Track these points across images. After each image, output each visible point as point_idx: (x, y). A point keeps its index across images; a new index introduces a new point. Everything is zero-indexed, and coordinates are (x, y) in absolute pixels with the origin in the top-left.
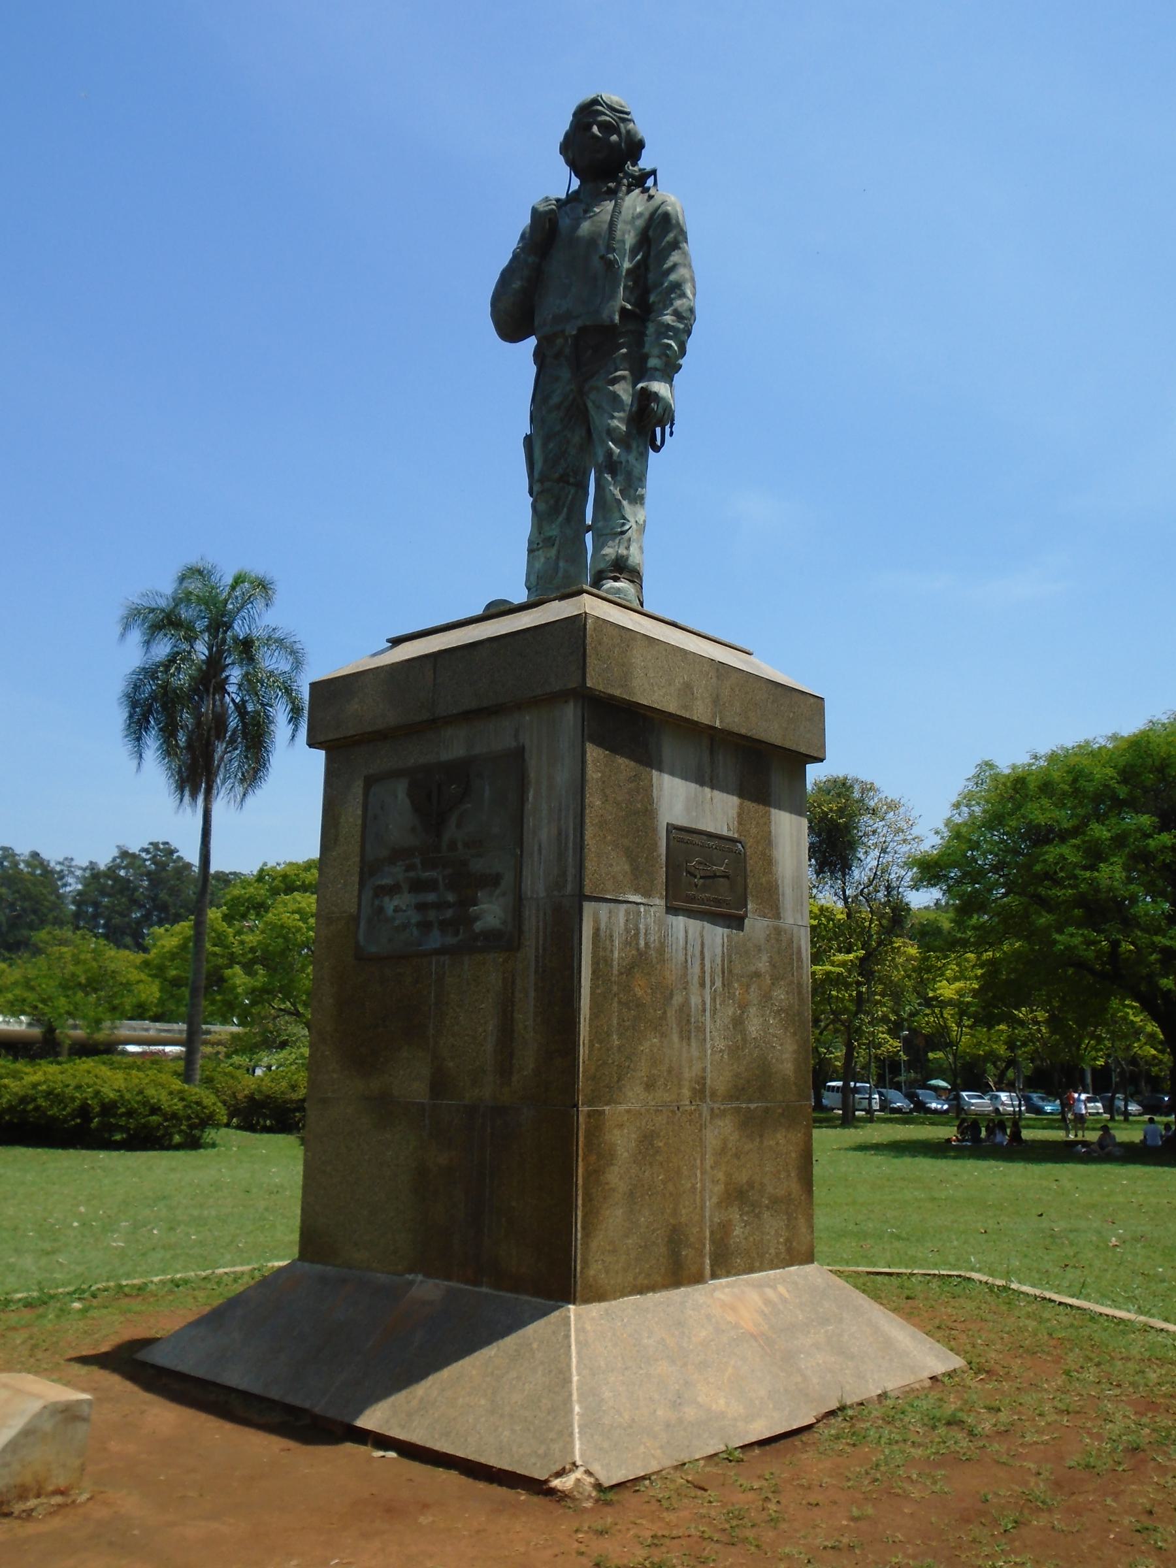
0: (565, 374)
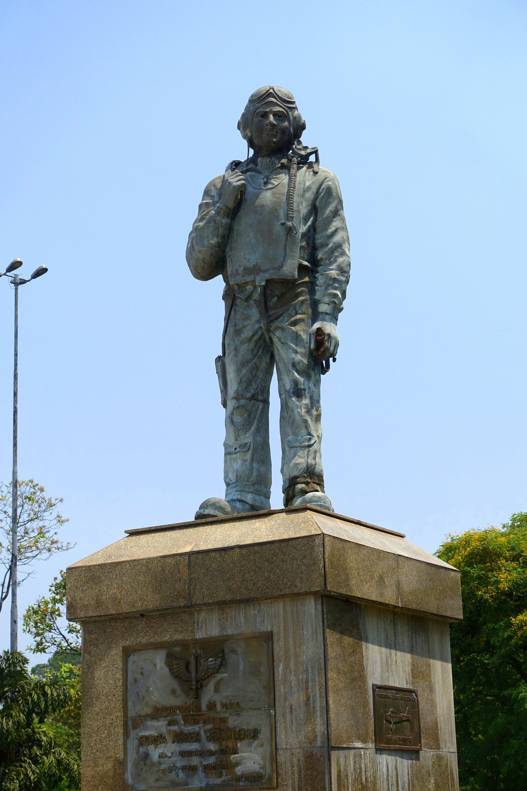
0: (255, 313)
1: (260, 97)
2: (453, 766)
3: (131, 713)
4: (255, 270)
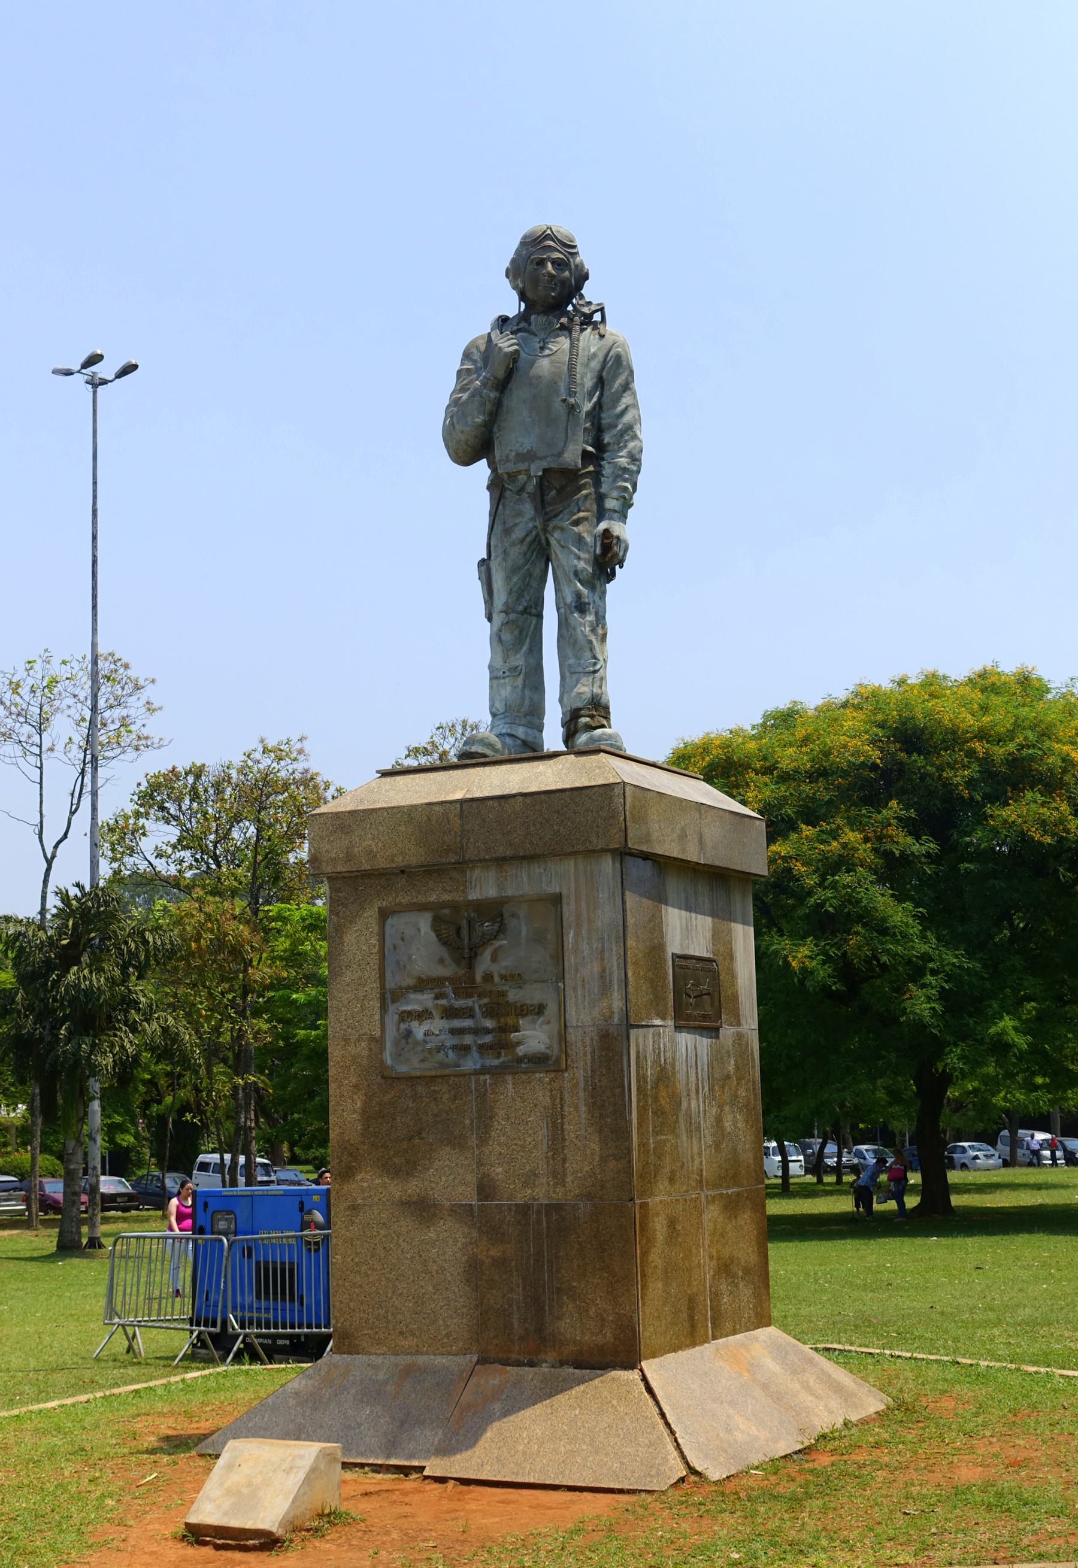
0: (528, 509)
1: (535, 240)
2: (754, 1045)
3: (390, 984)
4: (529, 457)
